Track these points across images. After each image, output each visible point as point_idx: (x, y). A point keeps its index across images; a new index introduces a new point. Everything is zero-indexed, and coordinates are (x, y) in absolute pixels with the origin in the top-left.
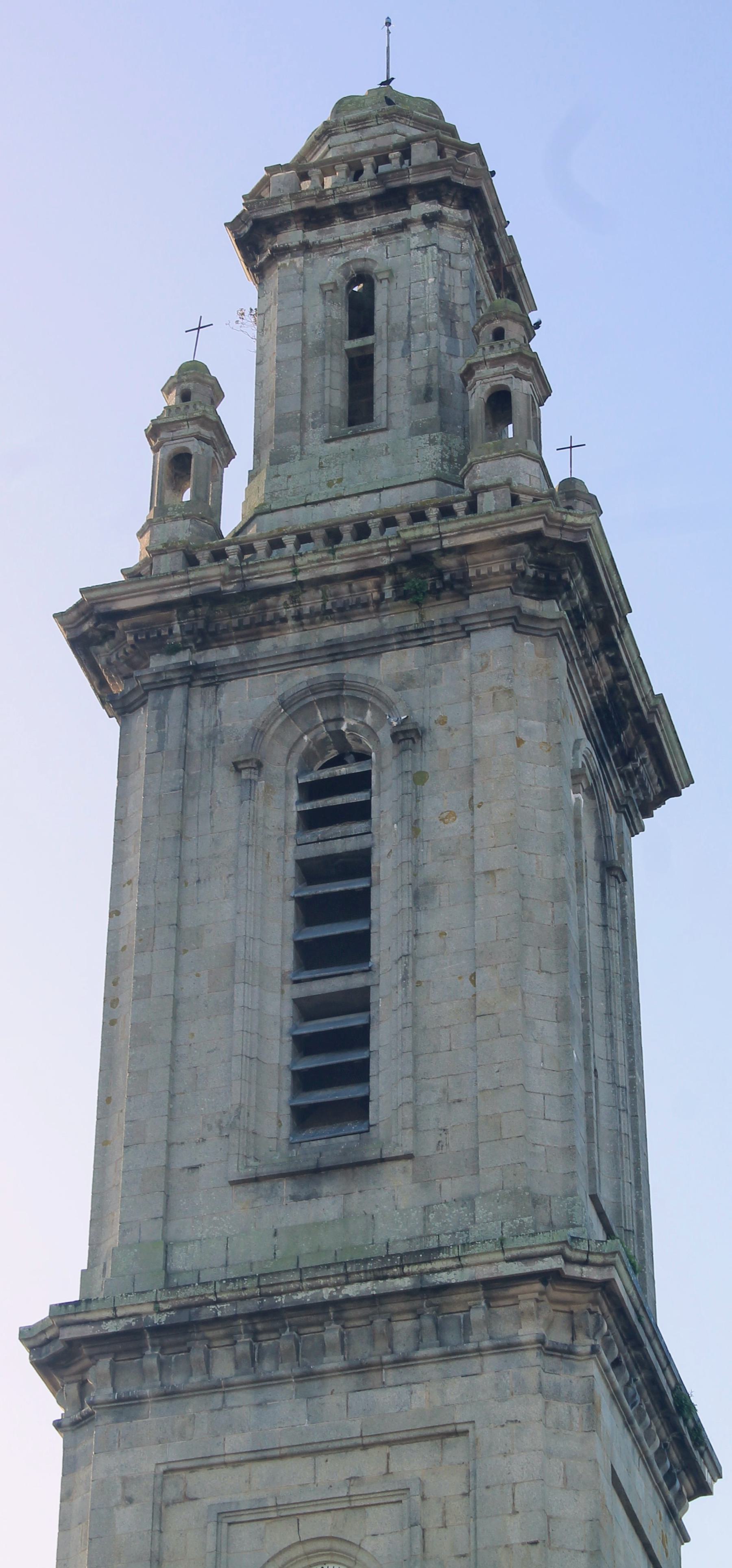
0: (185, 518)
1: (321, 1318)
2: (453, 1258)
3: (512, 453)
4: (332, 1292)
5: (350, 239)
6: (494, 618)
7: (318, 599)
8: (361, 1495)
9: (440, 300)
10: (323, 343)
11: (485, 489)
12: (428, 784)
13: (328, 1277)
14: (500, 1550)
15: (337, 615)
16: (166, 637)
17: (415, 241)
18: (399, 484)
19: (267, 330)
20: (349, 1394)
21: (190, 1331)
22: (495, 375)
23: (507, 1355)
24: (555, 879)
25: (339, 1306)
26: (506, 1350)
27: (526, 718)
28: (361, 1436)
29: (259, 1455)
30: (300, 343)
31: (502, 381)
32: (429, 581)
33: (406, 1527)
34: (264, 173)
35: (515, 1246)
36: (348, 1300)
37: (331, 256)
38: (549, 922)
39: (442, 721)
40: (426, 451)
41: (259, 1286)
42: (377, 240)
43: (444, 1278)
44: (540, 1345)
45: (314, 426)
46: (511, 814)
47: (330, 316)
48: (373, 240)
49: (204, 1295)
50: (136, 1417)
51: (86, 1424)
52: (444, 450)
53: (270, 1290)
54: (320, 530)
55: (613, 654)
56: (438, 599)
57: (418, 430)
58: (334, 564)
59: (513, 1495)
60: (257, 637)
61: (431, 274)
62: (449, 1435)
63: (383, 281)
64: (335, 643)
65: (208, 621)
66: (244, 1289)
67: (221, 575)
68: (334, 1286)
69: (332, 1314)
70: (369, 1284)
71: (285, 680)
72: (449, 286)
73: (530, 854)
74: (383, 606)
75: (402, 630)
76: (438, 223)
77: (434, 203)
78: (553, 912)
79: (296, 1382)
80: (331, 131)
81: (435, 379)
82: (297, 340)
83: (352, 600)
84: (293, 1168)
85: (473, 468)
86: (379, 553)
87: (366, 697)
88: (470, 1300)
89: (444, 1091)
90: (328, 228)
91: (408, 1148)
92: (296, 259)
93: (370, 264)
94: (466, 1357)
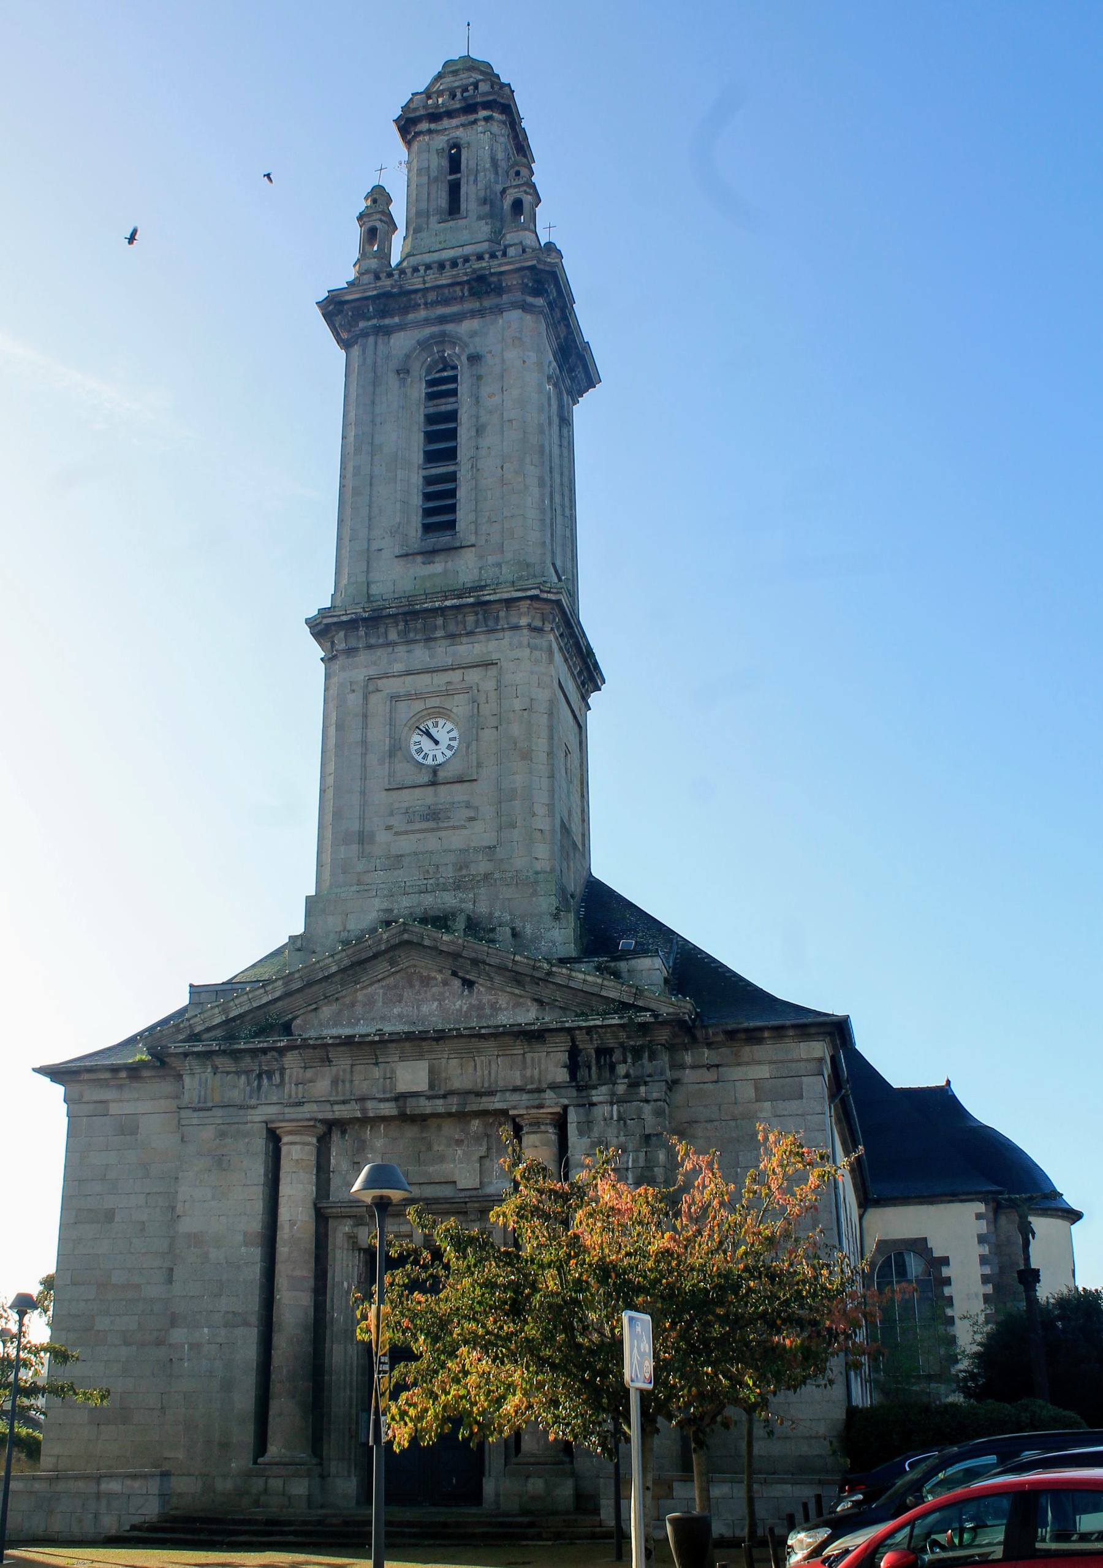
0: (375, 258)
6: (514, 305)
11: (511, 246)
17: (480, 129)
22: (516, 193)
25: (443, 610)
31: (518, 195)
36: (447, 607)
43: (488, 598)
62: (489, 664)
84: (424, 550)
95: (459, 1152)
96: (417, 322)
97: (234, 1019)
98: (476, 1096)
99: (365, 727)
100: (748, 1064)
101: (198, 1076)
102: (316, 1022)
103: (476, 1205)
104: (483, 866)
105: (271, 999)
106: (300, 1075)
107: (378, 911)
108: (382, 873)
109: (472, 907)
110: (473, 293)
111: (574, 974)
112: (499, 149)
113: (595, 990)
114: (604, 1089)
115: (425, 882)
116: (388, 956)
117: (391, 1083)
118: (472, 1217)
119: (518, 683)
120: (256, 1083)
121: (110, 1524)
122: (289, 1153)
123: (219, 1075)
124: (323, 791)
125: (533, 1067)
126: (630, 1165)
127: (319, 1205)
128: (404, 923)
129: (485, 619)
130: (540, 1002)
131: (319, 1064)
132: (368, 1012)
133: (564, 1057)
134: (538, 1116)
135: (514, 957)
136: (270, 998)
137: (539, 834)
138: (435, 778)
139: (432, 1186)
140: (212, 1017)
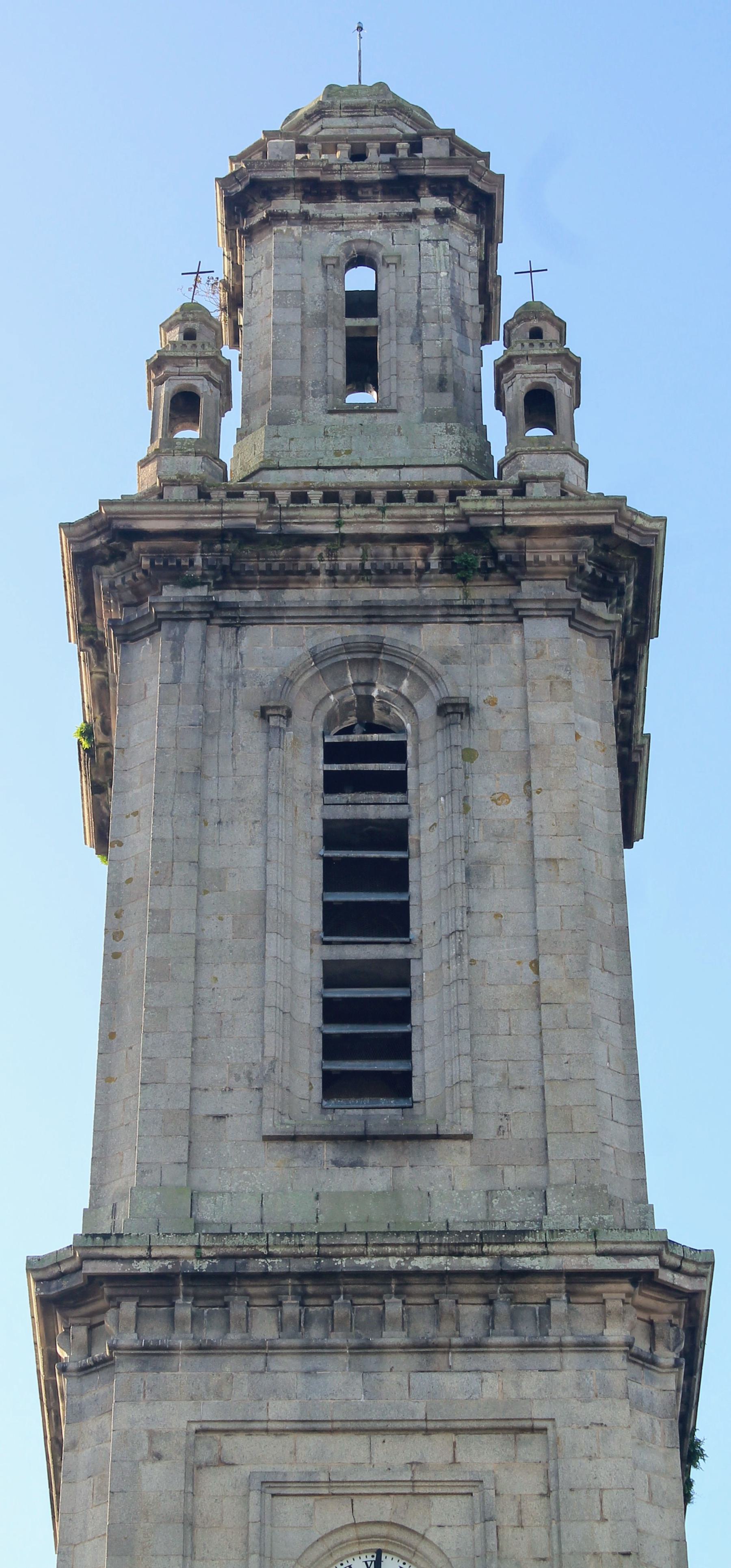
0: (197, 454)
1: (380, 1289)
2: (539, 1243)
3: (560, 450)
4: (399, 1262)
5: (354, 219)
7: (357, 557)
8: (427, 1481)
9: (451, 296)
10: (325, 315)
11: (536, 479)
12: (477, 762)
13: (397, 1245)
14: (588, 1557)
15: (374, 577)
16: (185, 568)
17: (425, 233)
18: (422, 464)
19: (256, 293)
20: (411, 1374)
21: (230, 1284)
22: (536, 372)
23: (591, 1355)
24: (614, 880)
26: (589, 1349)
27: (581, 714)
28: (426, 1420)
29: (307, 1426)
30: (299, 311)
31: (545, 379)
32: (480, 559)
33: (477, 1522)
34: (262, 137)
35: (610, 1240)
37: (331, 232)
38: (610, 922)
39: (492, 702)
40: (443, 439)
41: (318, 1245)
42: (381, 225)
43: (527, 1263)
44: (627, 1348)
46: (574, 805)
47: (332, 290)
48: (377, 224)
49: (255, 1246)
50: (163, 1369)
51: (97, 1371)
52: (462, 441)
53: (330, 1251)
54: (350, 491)
55: (628, 678)
56: (486, 579)
58: (382, 523)
59: (601, 1502)
61: (443, 268)
62: (523, 1430)
63: (391, 266)
64: (374, 604)
65: (234, 558)
66: (301, 1246)
67: (258, 512)
68: (402, 1256)
69: (393, 1286)
70: (442, 1258)
71: (314, 634)
72: (459, 284)
73: (589, 850)
74: (425, 577)
75: (448, 603)
76: (449, 220)
77: (446, 200)
78: (613, 913)
79: (351, 1354)
80: (325, 112)
81: (449, 370)
82: (295, 307)
83: (394, 565)
84: (336, 1131)
85: (517, 458)
86: (433, 519)
87: (406, 665)
88: (550, 1292)
89: (504, 1076)
90: (327, 204)
92: (293, 228)
93: (374, 247)
94: (544, 1351)
112: (467, 284)
119: (604, 1485)
129: (513, 1319)
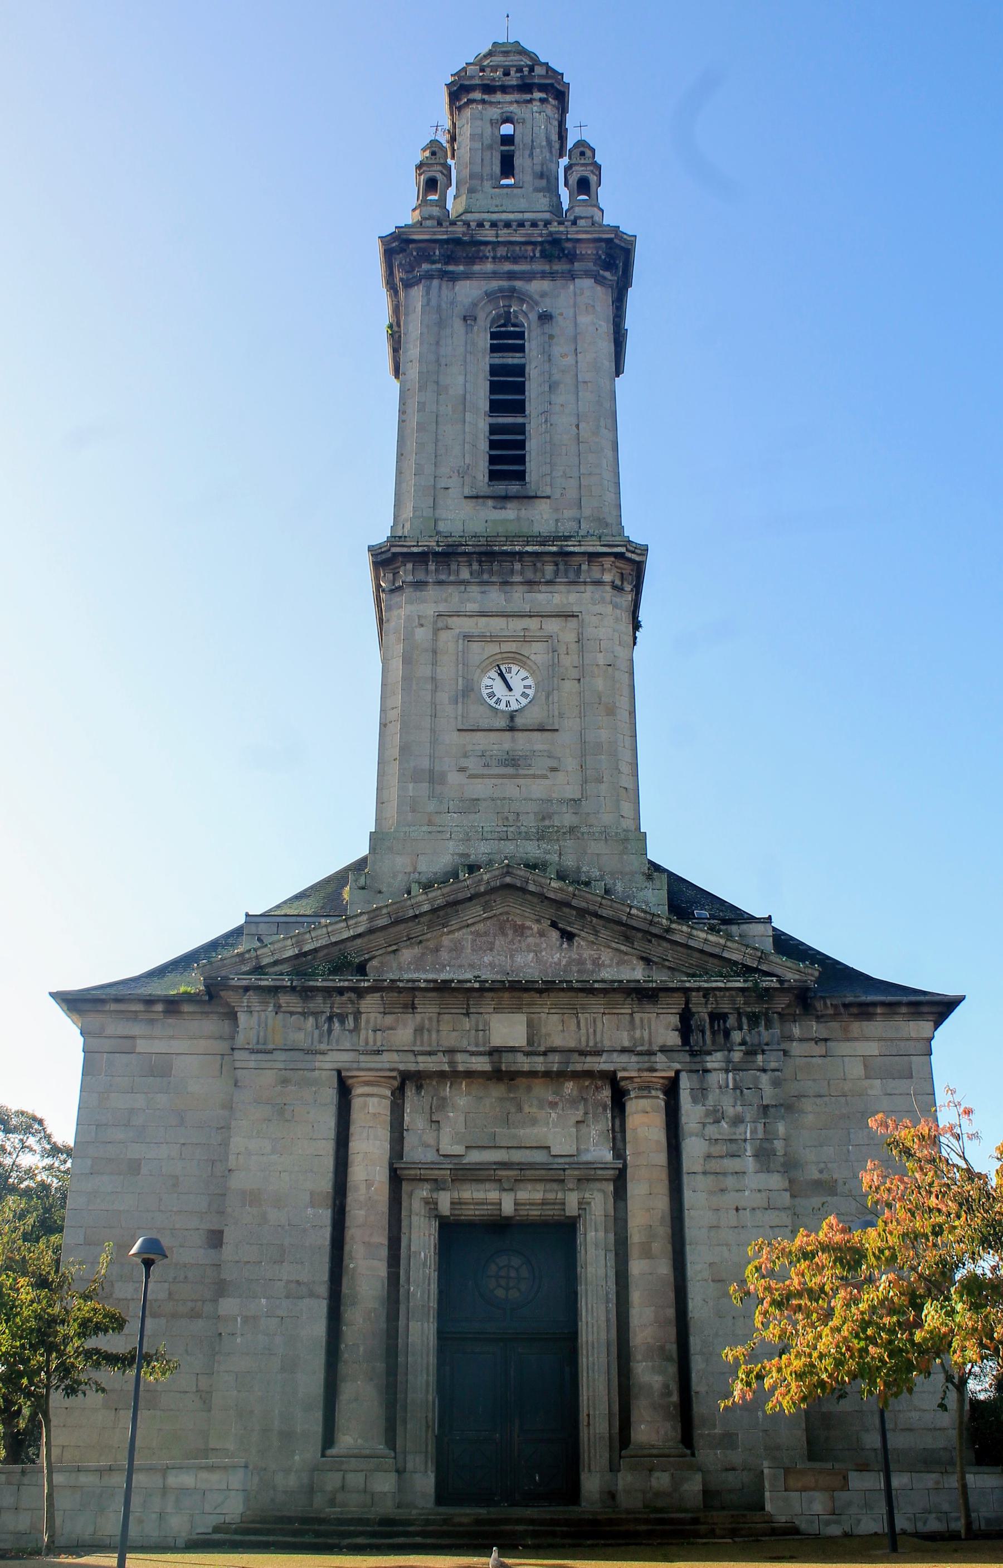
0: (436, 206)
1: (512, 559)
6: (587, 274)
17: (535, 109)
25: (521, 554)
31: (586, 174)
36: (527, 552)
39: (561, 314)
43: (572, 549)
45: (487, 180)
53: (491, 543)
57: (537, 190)
60: (473, 263)
83: (520, 255)
84: (495, 494)
91: (548, 494)
93: (513, 115)
95: (553, 1115)
96: (485, 273)
97: (305, 954)
98: (580, 1055)
99: (434, 663)
100: (856, 1039)
101: (255, 1014)
102: (395, 965)
103: (576, 1173)
104: (567, 819)
105: (352, 934)
106: (379, 1022)
107: (453, 855)
108: (455, 815)
109: (557, 859)
110: (546, 256)
111: (695, 932)
113: (716, 951)
114: (719, 1055)
115: (505, 829)
116: (482, 900)
117: (484, 1035)
118: (571, 1186)
120: (326, 1026)
121: (178, 1525)
122: (365, 1105)
123: (280, 1016)
124: (383, 725)
125: (642, 1028)
126: (748, 1136)
127: (395, 1166)
128: (508, 865)
130: (647, 961)
131: (400, 1010)
132: (454, 959)
133: (675, 1020)
134: (650, 1079)
135: (630, 910)
136: (352, 933)
137: (624, 791)
138: (512, 724)
139: (522, 1150)
140: (284, 948)
